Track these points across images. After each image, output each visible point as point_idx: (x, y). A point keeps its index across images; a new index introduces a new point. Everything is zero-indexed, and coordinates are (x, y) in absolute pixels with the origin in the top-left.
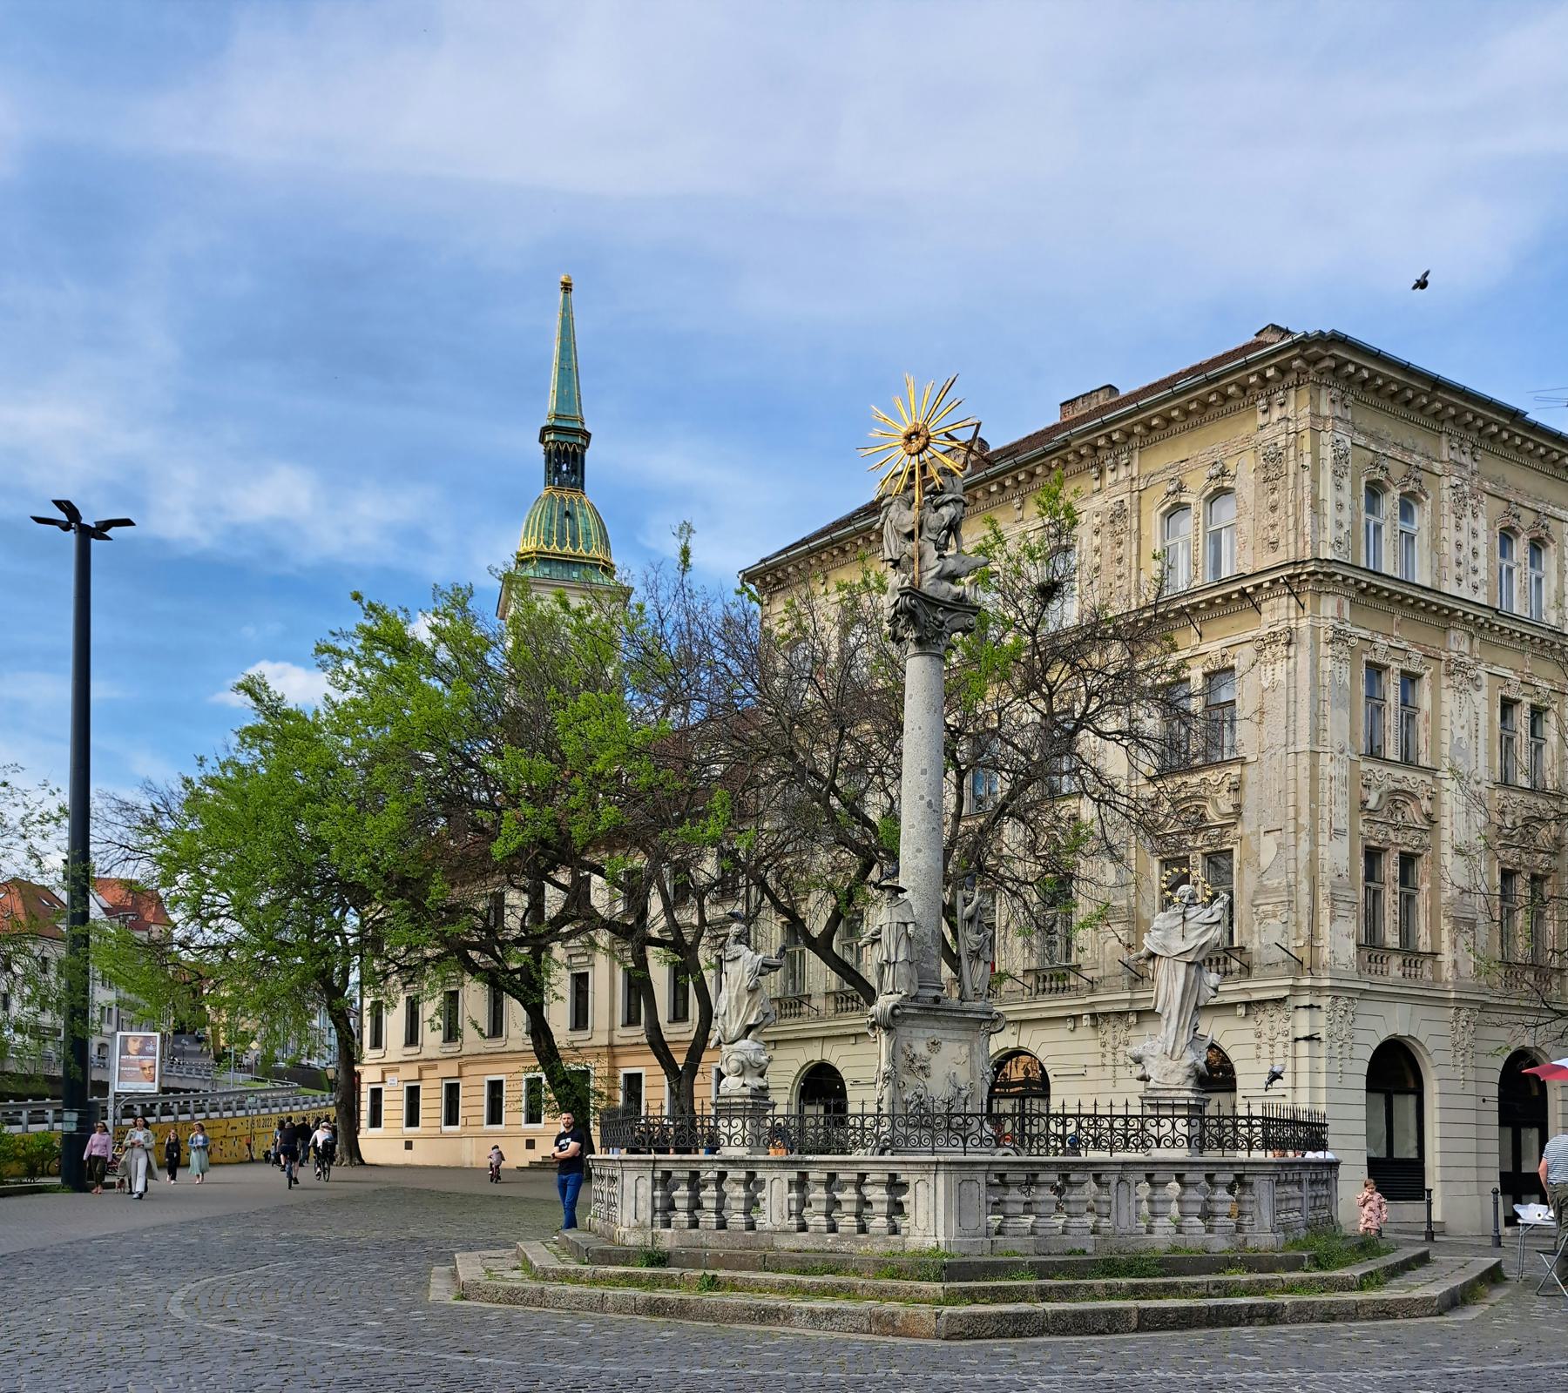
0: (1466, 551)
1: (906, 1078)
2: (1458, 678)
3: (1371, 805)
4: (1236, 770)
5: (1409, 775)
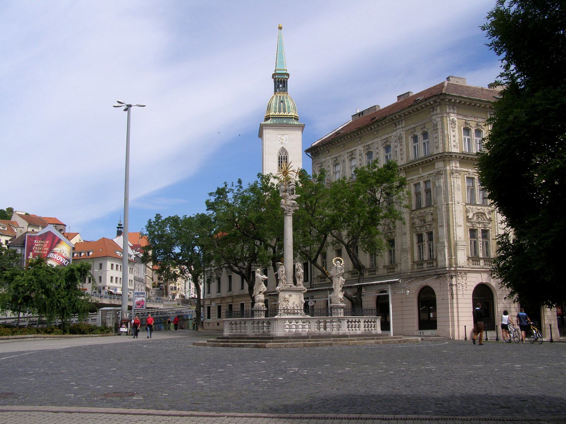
1: (284, 303)
3: (470, 217)
4: (432, 209)
5: (483, 208)
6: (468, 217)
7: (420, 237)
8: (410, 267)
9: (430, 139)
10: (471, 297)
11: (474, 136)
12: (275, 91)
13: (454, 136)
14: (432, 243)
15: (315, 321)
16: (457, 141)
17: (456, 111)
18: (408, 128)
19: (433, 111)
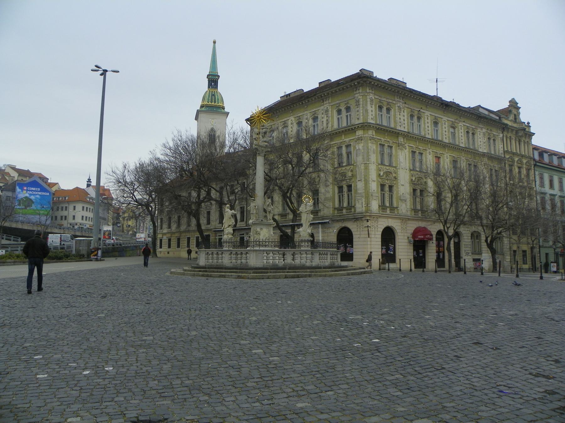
0: (402, 120)
2: (401, 147)
3: (381, 175)
4: (352, 167)
5: (390, 168)
7: (340, 188)
8: (331, 212)
12: (209, 87)
14: (351, 194)
15: (291, 253)
17: (373, 92)
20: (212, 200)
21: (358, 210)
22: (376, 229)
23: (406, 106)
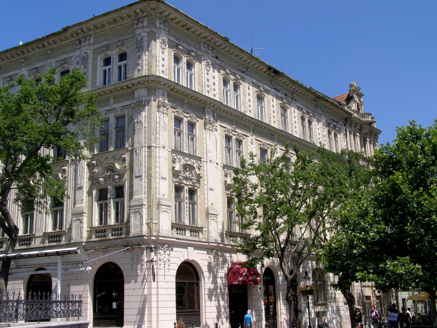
6: (173, 168)
9: (129, 61)
10: (174, 279)
11: (186, 68)
13: (163, 59)
14: (123, 202)
16: (166, 67)
17: (167, 29)
18: (97, 46)
19: (137, 24)
20: (344, 293)
21: (133, 232)
22: (167, 265)
23: (218, 61)
